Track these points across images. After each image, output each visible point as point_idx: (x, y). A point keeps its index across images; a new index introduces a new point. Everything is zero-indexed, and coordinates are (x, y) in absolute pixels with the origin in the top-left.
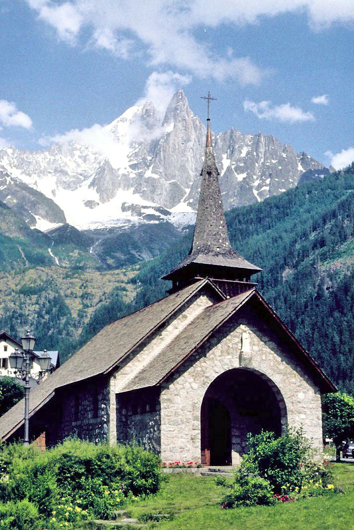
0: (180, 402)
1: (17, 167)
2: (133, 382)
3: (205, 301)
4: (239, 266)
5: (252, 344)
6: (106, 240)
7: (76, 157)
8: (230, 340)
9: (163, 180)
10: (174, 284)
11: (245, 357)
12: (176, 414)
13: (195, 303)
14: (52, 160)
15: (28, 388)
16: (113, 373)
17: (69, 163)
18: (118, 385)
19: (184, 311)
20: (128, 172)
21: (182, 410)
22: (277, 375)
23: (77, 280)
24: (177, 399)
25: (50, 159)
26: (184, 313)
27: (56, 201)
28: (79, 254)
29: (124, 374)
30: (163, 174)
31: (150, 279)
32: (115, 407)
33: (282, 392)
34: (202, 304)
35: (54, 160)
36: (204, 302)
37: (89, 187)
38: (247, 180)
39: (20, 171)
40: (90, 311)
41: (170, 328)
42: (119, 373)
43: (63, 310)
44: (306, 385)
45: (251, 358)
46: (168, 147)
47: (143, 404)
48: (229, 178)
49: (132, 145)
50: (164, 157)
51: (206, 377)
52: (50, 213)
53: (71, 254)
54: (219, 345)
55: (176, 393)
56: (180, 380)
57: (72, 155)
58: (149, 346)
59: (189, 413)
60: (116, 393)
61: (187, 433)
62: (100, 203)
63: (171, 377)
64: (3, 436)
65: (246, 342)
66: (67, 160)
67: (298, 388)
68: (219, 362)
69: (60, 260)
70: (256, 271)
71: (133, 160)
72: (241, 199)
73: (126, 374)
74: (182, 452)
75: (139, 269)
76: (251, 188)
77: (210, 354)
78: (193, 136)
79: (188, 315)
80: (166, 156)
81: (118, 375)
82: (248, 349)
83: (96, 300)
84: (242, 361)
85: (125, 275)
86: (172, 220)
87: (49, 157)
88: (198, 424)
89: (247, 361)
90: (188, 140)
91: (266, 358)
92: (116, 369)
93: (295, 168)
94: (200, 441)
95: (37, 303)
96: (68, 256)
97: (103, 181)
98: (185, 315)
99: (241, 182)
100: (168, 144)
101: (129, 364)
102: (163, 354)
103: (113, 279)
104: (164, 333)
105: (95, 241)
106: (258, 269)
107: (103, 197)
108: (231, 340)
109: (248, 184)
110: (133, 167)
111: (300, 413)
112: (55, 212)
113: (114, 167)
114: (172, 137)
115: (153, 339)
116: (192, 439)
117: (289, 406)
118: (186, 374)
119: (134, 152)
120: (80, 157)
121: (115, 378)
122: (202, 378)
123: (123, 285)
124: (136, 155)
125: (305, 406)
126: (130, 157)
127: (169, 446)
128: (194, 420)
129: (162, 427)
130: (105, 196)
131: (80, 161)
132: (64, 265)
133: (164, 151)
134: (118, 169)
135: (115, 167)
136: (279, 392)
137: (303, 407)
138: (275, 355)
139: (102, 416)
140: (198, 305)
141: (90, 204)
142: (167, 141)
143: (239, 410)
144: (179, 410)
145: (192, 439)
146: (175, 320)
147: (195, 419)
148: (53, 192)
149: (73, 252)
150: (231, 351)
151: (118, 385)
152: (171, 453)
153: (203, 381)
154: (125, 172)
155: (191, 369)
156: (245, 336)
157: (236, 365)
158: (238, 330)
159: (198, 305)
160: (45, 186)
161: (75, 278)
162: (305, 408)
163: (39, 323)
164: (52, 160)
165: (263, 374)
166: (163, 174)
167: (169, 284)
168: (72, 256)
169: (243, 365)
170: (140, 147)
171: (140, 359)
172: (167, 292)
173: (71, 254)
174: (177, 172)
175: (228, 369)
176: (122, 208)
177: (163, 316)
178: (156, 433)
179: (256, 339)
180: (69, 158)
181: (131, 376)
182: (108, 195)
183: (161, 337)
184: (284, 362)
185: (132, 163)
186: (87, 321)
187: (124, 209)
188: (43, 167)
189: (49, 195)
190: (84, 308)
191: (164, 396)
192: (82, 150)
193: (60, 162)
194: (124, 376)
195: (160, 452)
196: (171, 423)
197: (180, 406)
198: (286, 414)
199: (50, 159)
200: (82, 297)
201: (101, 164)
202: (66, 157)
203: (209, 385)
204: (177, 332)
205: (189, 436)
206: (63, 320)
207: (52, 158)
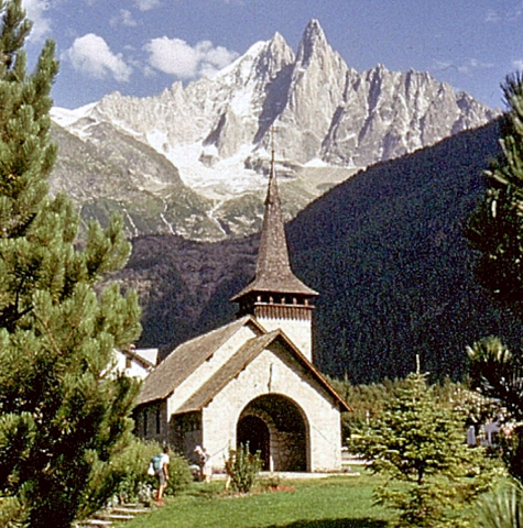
2: (185, 405)
4: (294, 289)
6: (229, 202)
23: (195, 251)
27: (168, 156)
28: (197, 219)
40: (211, 287)
43: (180, 285)
52: (162, 171)
53: (187, 220)
62: (221, 158)
64: (173, 396)
69: (174, 226)
78: (332, 75)
83: (216, 274)
85: (251, 245)
90: (326, 81)
93: (472, 95)
95: (149, 278)
96: (184, 222)
109: (396, 132)
112: (168, 170)
117: (311, 423)
123: (249, 256)
147: (231, 434)
148: (165, 146)
149: (189, 216)
157: (266, 392)
163: (151, 302)
168: (188, 223)
173: (187, 220)
189: (160, 150)
200: (201, 271)
206: (180, 298)
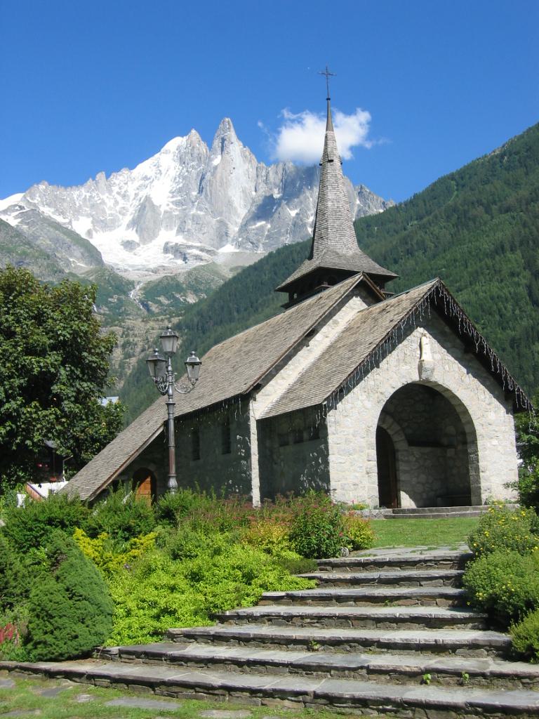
0: (350, 426)
1: (49, 205)
3: (358, 302)
5: (433, 352)
7: (114, 193)
8: (406, 346)
9: (209, 218)
10: (291, 297)
11: (427, 366)
12: (347, 441)
13: (347, 305)
14: (88, 197)
15: (171, 404)
16: (43, 482)
17: (107, 200)
18: (260, 408)
19: (334, 315)
20: (171, 209)
21: (353, 436)
22: (463, 390)
24: (348, 421)
25: (86, 196)
26: (334, 318)
28: (118, 299)
29: (266, 395)
30: (210, 210)
31: (198, 325)
32: (256, 437)
33: (471, 412)
34: (356, 306)
35: (90, 197)
36: (357, 304)
37: (128, 226)
38: (301, 216)
39: (53, 210)
40: (133, 361)
41: (318, 337)
42: (260, 393)
44: (495, 402)
45: (434, 369)
46: (214, 181)
47: (301, 433)
48: (281, 214)
49: (175, 179)
50: (210, 191)
51: (381, 393)
52: (86, 254)
54: (394, 353)
55: (345, 415)
56: (349, 398)
57: (110, 192)
58: (294, 359)
59: (362, 440)
60: (257, 418)
61: (361, 465)
63: (341, 393)
65: (426, 348)
66: (105, 197)
67: (488, 407)
68: (396, 372)
70: (390, 278)
71: (176, 197)
72: (294, 236)
73: (268, 395)
74: (355, 489)
75: (184, 314)
76: (304, 225)
77: (383, 364)
79: (339, 320)
80: (213, 191)
81: (259, 396)
82: (427, 358)
83: (138, 350)
84: (423, 373)
86: (220, 260)
87: (84, 194)
88: (373, 453)
89: (429, 373)
91: (449, 369)
92: (257, 388)
94: (376, 475)
97: (145, 219)
98: (336, 320)
99: (294, 218)
100: (215, 178)
101: (271, 383)
102: (315, 366)
103: (157, 326)
104: (312, 343)
105: (136, 284)
106: (394, 275)
107: (143, 238)
108: (407, 347)
109: (301, 220)
110: (177, 203)
111: (492, 438)
112: (92, 254)
113: (155, 203)
114: (219, 170)
115: (299, 351)
116: (368, 473)
117: (479, 430)
118: (356, 390)
119: (178, 187)
120: (118, 193)
121: (255, 400)
122: (376, 395)
124: (180, 190)
125: (496, 429)
126: (173, 192)
127: (340, 483)
128: (369, 449)
129: (331, 458)
130: (146, 235)
131: (119, 198)
132: (102, 311)
133: (211, 186)
134: (160, 206)
135: (156, 202)
136: (466, 411)
137: (494, 430)
138: (459, 365)
139: (239, 450)
140: (351, 307)
141: (129, 245)
142: (213, 174)
143: (423, 438)
144: (351, 436)
145: (368, 473)
146: (325, 327)
150: (408, 359)
151: (260, 408)
152: (343, 492)
153: (378, 398)
154: (167, 208)
155: (362, 383)
156: (425, 340)
158: (415, 333)
159: (351, 307)
160: (81, 226)
161: (116, 326)
162: (496, 432)
164: (88, 197)
165: (447, 390)
166: (210, 210)
167: (285, 297)
168: (111, 302)
169: (424, 376)
170: (184, 182)
171: (285, 376)
172: (282, 306)
174: (224, 208)
175: (406, 383)
176: (164, 248)
177: (309, 323)
178: (322, 467)
179: (437, 345)
180: (107, 194)
181: (275, 397)
182: (149, 235)
183: (308, 348)
184: (470, 375)
185: (174, 199)
186: (129, 372)
187: (166, 250)
188: (78, 205)
190: (126, 359)
191: (331, 417)
192: (121, 185)
193: (96, 199)
194: (266, 397)
195: (328, 491)
196: (342, 453)
197: (351, 431)
198: (475, 439)
199: (86, 196)
201: (142, 201)
202: (103, 194)
203: (384, 403)
204: (327, 342)
205: (364, 468)
207: (88, 194)
